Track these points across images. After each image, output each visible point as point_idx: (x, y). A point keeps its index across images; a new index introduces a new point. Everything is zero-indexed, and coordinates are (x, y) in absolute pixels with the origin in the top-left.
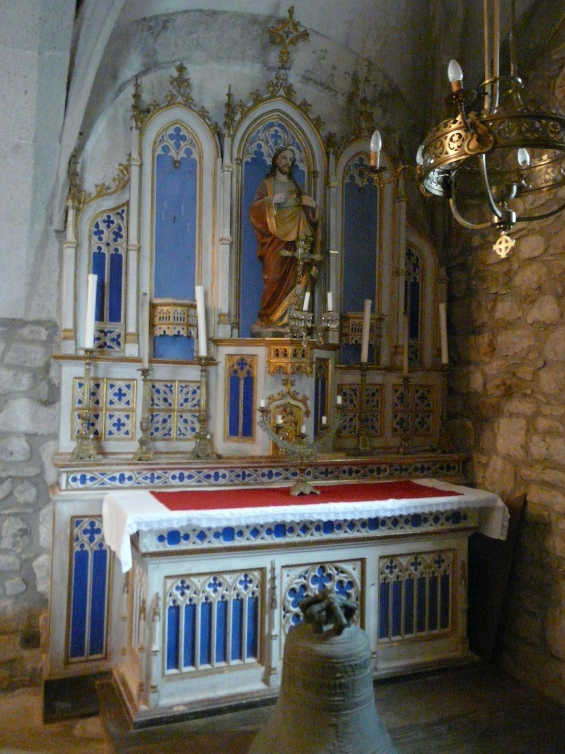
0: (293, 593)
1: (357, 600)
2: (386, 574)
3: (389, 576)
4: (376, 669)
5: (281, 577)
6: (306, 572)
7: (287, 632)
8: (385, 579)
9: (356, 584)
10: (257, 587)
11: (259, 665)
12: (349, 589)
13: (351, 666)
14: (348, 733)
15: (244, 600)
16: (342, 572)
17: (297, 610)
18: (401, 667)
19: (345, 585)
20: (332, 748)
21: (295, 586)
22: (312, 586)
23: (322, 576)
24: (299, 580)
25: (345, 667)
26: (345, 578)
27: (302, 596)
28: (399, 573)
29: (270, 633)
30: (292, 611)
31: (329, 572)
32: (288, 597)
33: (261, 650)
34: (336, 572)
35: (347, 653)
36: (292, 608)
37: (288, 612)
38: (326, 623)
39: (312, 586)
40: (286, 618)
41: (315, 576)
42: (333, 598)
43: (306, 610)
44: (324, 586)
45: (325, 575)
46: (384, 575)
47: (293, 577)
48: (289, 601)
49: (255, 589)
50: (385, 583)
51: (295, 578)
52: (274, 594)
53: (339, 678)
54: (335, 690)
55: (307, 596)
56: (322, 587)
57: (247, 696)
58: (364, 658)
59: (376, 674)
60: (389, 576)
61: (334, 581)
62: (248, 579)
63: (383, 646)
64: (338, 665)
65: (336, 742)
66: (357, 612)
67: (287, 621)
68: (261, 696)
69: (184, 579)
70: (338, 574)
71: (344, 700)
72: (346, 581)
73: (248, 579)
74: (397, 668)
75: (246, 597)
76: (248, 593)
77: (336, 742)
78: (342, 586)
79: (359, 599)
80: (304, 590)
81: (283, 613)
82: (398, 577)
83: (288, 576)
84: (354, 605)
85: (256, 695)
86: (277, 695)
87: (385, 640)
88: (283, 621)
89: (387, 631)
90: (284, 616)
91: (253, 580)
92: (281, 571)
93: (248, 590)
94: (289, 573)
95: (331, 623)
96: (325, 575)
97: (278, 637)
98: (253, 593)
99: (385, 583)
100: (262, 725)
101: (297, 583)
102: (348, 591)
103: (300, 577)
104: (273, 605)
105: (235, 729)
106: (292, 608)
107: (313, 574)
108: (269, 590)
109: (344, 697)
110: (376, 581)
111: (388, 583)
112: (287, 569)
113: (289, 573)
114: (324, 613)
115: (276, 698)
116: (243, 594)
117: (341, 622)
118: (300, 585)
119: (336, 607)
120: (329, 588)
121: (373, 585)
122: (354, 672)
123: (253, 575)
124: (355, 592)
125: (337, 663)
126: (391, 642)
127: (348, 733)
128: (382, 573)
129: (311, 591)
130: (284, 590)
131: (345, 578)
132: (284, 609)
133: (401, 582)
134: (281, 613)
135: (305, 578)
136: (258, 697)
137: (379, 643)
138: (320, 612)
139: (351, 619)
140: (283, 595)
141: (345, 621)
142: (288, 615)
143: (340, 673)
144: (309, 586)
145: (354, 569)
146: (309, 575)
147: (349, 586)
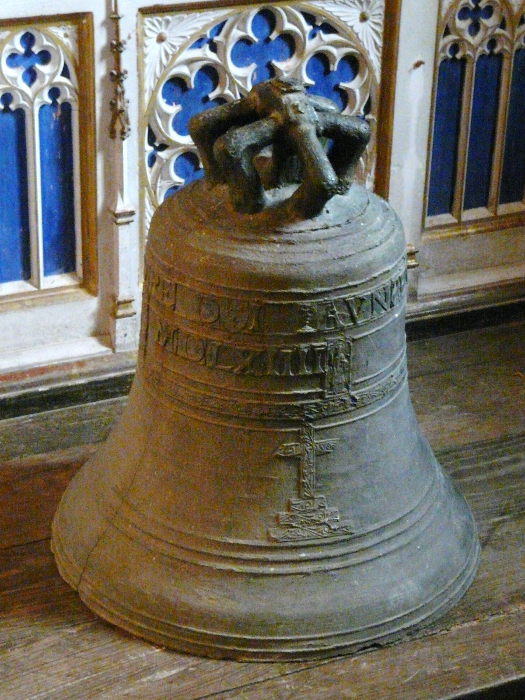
0: (178, 92)
1: (368, 109)
2: (458, 32)
3: (468, 37)
4: (413, 296)
5: (140, 45)
6: (219, 29)
7: (161, 201)
8: (455, 48)
9: (367, 63)
10: (65, 73)
11: (82, 292)
12: (345, 80)
13: (346, 302)
14: (331, 477)
15: (28, 113)
16: (328, 28)
17: (187, 140)
18: (486, 288)
19: (334, 67)
20: (283, 513)
21: (184, 70)
22: (234, 70)
23: (268, 40)
24: (197, 53)
25: (329, 307)
26: (336, 45)
27: (206, 99)
28: (499, 31)
29: (109, 208)
30: (177, 145)
31: (288, 26)
32: (162, 102)
33: (85, 258)
34: (308, 28)
35: (335, 268)
36: (174, 136)
37: (163, 147)
38: (274, 184)
39: (234, 70)
40: (156, 165)
41: (245, 41)
42: (295, 107)
43: (211, 144)
44: (272, 70)
45: (274, 36)
46: (452, 37)
47: (177, 43)
48: (165, 116)
49: (60, 79)
50: (454, 59)
51: (182, 48)
52: (119, 95)
53: (308, 337)
54: (296, 368)
55: (221, 100)
56: (266, 73)
57: (54, 374)
58: (386, 282)
59: (414, 307)
60: (468, 37)
61: (301, 55)
62: (36, 49)
63: (437, 235)
64: (307, 302)
65: (294, 500)
66: (370, 147)
67: (162, 173)
68: (91, 374)
69: (31, 29)
70: (313, 35)
71: (321, 395)
72: (338, 53)
73: (36, 49)
74: (472, 291)
75: (32, 103)
76: (38, 92)
77: (294, 500)
78: (327, 71)
79: (375, 107)
80: (209, 84)
81: (149, 149)
82: (492, 43)
83: (161, 39)
84: (363, 128)
85: (75, 371)
86: (134, 371)
87: (446, 218)
88: (150, 173)
89: (452, 199)
90: (153, 159)
91: (52, 53)
92: (140, 25)
93: (37, 84)
94: (162, 30)
95: (291, 181)
96: (274, 36)
97: (136, 218)
98: (54, 92)
99: (454, 59)
100: (92, 448)
101: (190, 62)
102: (343, 85)
103: (199, 43)
104: (118, 127)
105: (15, 461)
106: (174, 136)
107: (237, 34)
108: (103, 81)
109: (322, 386)
110: (428, 58)
111: (464, 60)
112: (156, 19)
113: (162, 30)
114: (267, 153)
115: (132, 376)
116: (23, 93)
117: (320, 175)
118: (198, 66)
119: (304, 135)
120: (286, 76)
121: (418, 65)
122: (353, 319)
123: (51, 37)
124: (364, 87)
125: (302, 296)
126: (460, 224)
127: (331, 477)
128: (447, 32)
129: (233, 82)
130: (149, 83)
131: (336, 45)
132: (152, 139)
133: (500, 56)
134: (142, 150)
135: (214, 47)
136: (81, 375)
137: (423, 229)
138: (254, 149)
139: (352, 169)
140: (147, 98)
141: (331, 176)
142: (162, 154)
143: (313, 324)
144: (227, 72)
145: (364, 18)
146: (227, 36)
147: (348, 69)
